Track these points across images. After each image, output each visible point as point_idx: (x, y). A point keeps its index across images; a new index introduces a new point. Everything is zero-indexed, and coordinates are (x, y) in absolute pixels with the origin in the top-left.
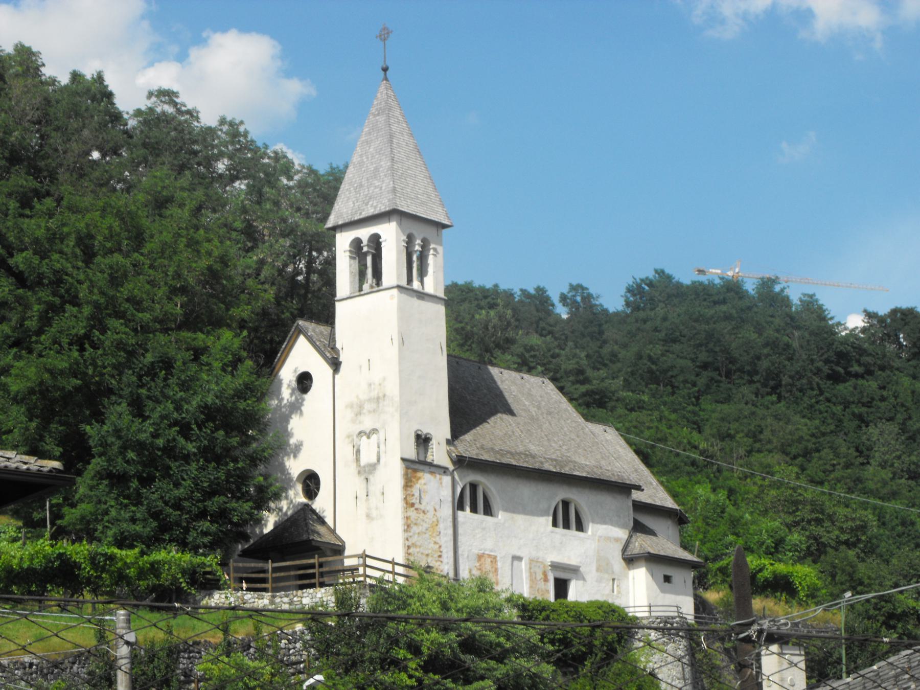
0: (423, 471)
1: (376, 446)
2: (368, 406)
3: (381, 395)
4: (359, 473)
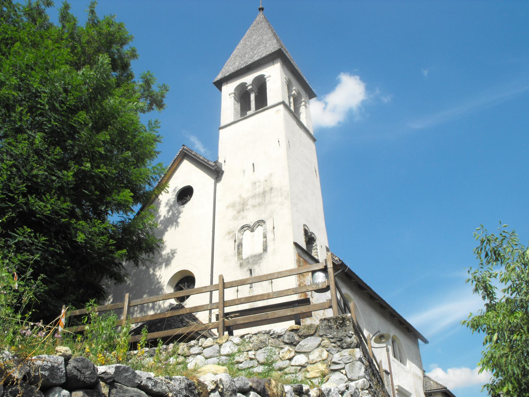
2: (251, 202)
3: (267, 189)
4: (241, 265)
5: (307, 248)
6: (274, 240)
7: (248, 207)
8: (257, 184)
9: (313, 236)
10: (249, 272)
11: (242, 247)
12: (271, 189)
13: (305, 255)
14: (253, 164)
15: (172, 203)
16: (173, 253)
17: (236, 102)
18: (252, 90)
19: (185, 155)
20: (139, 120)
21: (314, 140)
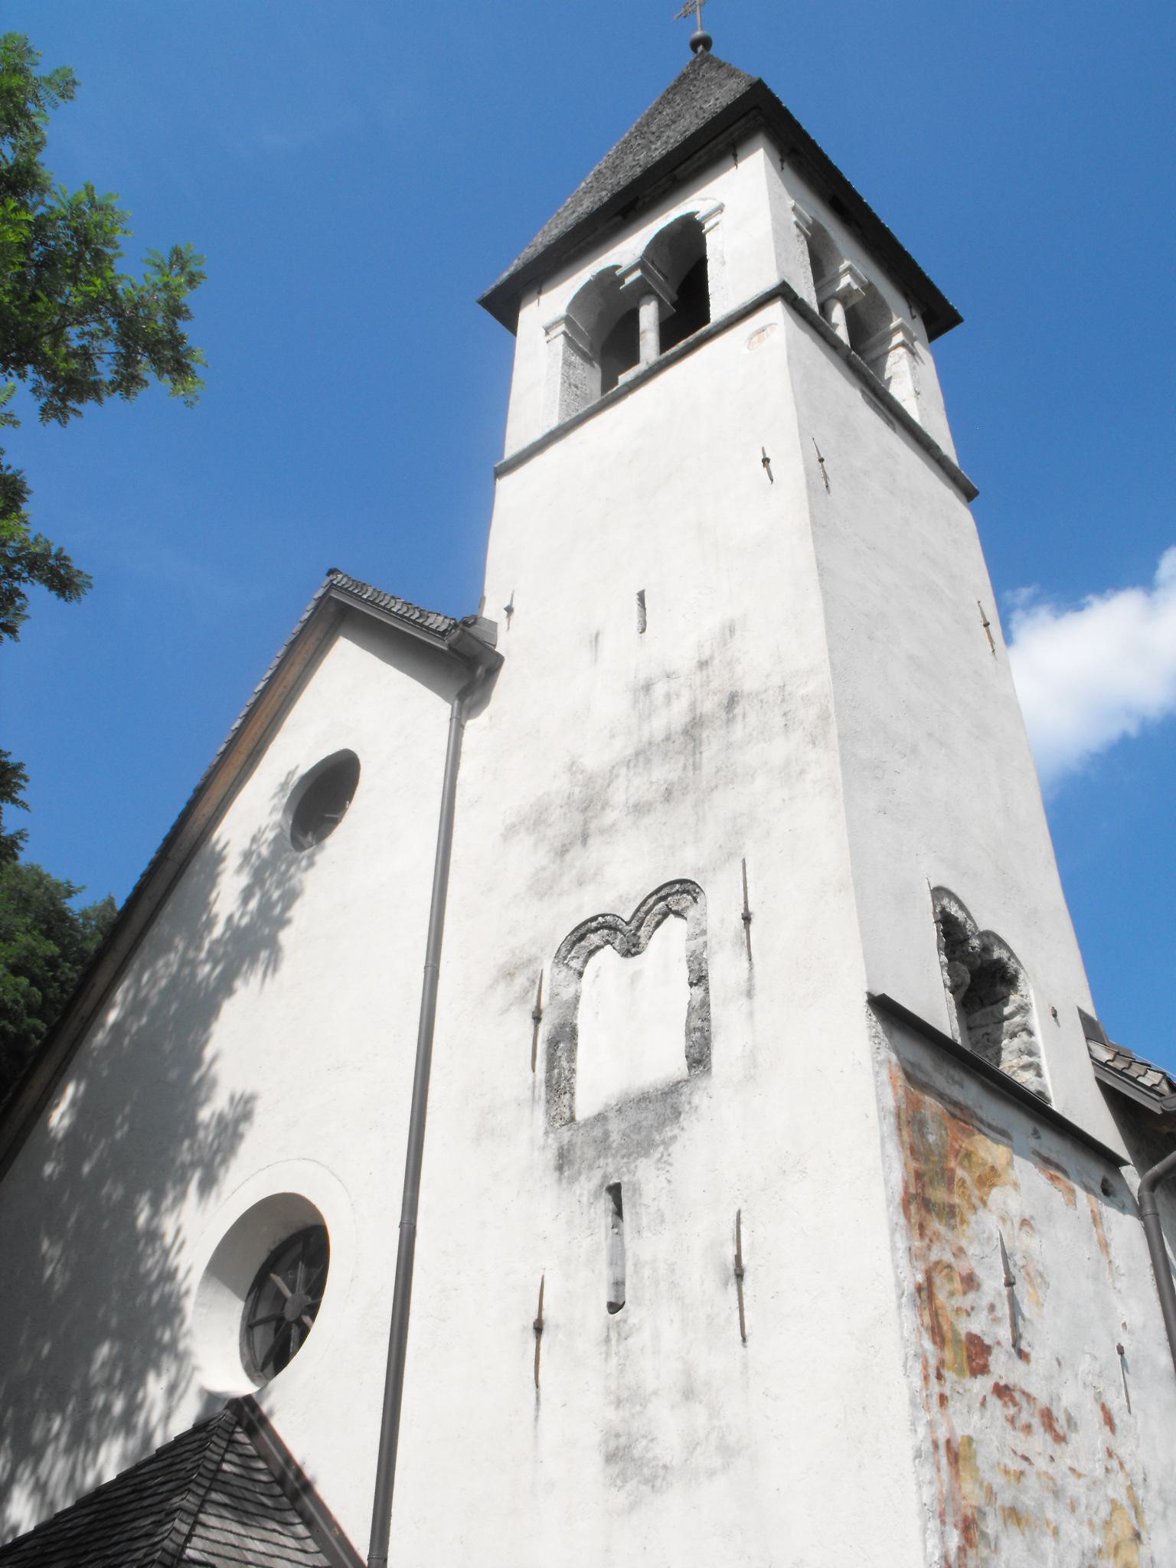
0: (1002, 1134)
1: (683, 974)
2: (620, 795)
3: (709, 705)
4: (564, 1160)
5: (968, 1028)
6: (749, 994)
7: (611, 816)
8: (660, 689)
9: (998, 953)
10: (606, 1203)
11: (572, 1051)
12: (732, 701)
13: (958, 1075)
14: (641, 597)
15: (265, 851)
17: (576, 359)
18: (642, 290)
19: (341, 614)
21: (968, 493)
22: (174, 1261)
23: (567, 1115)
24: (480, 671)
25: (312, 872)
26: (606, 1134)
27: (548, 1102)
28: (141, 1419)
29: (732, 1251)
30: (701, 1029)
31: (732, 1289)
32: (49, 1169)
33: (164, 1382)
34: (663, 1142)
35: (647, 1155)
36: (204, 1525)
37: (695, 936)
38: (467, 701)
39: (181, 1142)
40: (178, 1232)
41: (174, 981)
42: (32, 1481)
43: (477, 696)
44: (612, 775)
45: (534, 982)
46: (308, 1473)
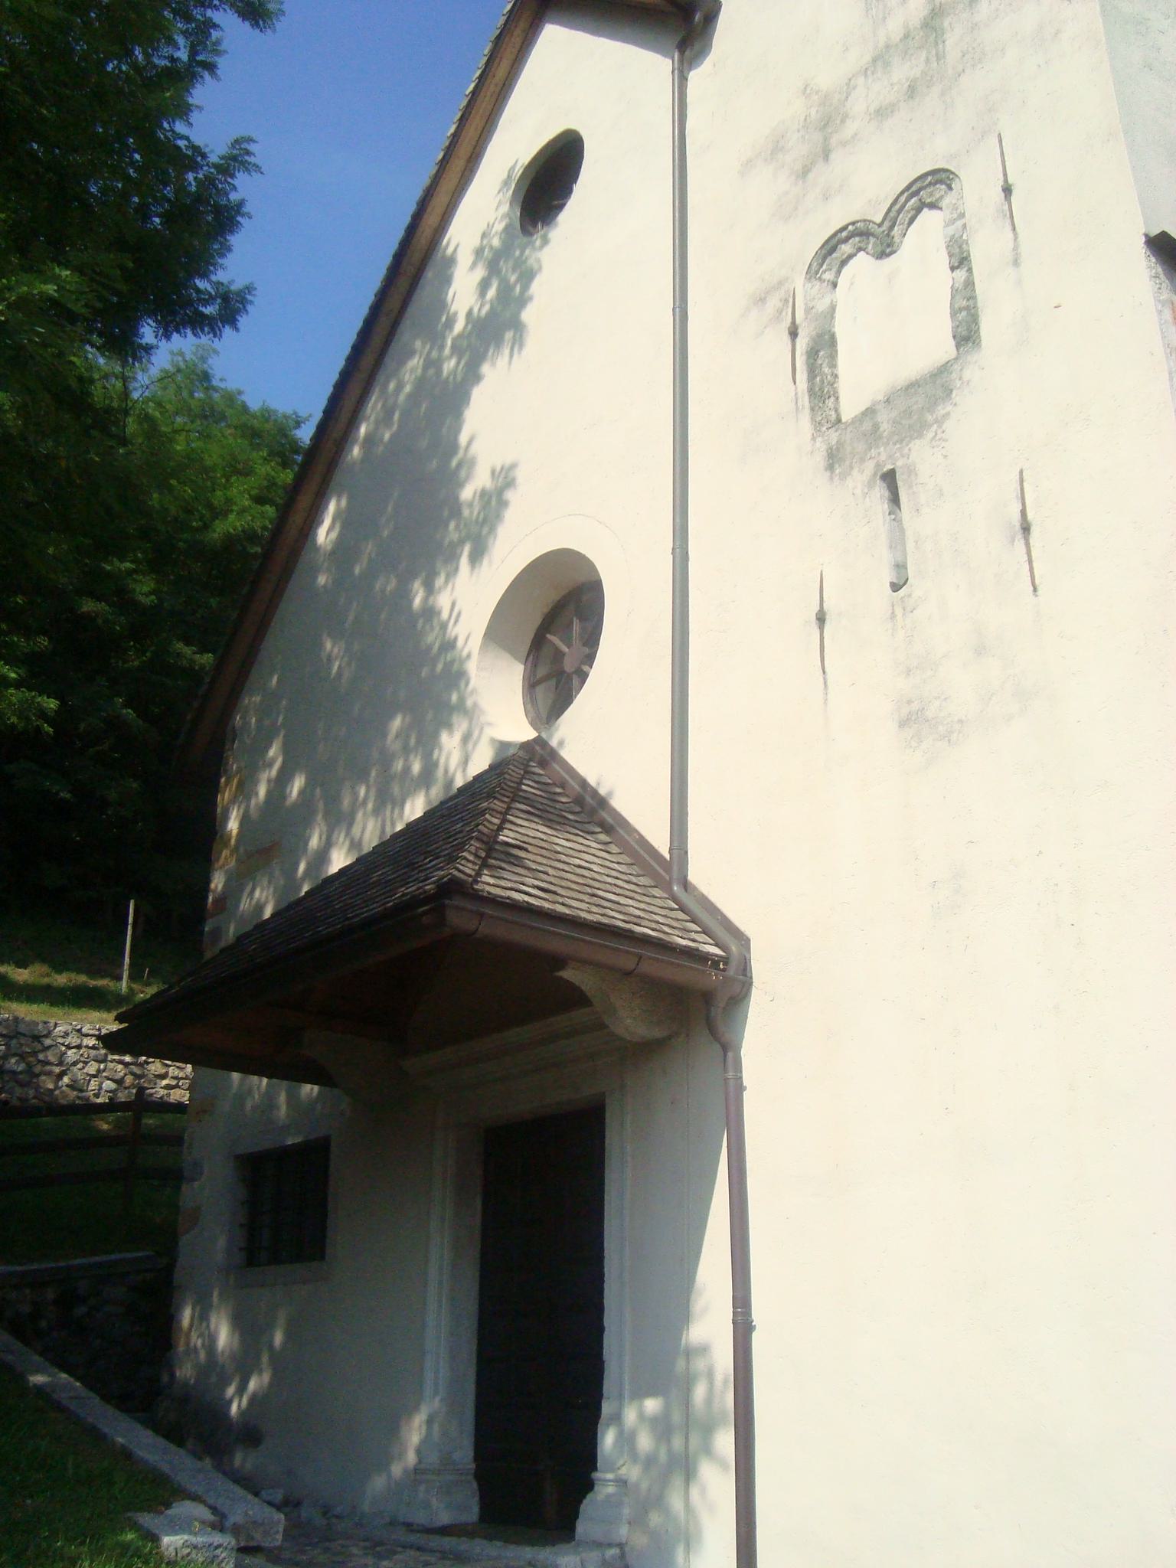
2: (858, 105)
4: (834, 459)
6: (1016, 262)
7: (851, 128)
10: (880, 491)
15: (496, 242)
16: (505, 479)
20: (252, 147)
22: (452, 631)
23: (834, 417)
24: (698, 17)
25: (547, 249)
26: (876, 427)
27: (812, 409)
28: (440, 772)
29: (1017, 508)
30: (967, 308)
31: (1020, 544)
32: (322, 580)
33: (458, 736)
34: (936, 421)
35: (920, 436)
36: (512, 823)
37: (953, 221)
38: (687, 53)
39: (447, 526)
40: (453, 605)
41: (420, 383)
42: (347, 843)
43: (697, 46)
44: (849, 86)
45: (786, 301)
46: (602, 791)
